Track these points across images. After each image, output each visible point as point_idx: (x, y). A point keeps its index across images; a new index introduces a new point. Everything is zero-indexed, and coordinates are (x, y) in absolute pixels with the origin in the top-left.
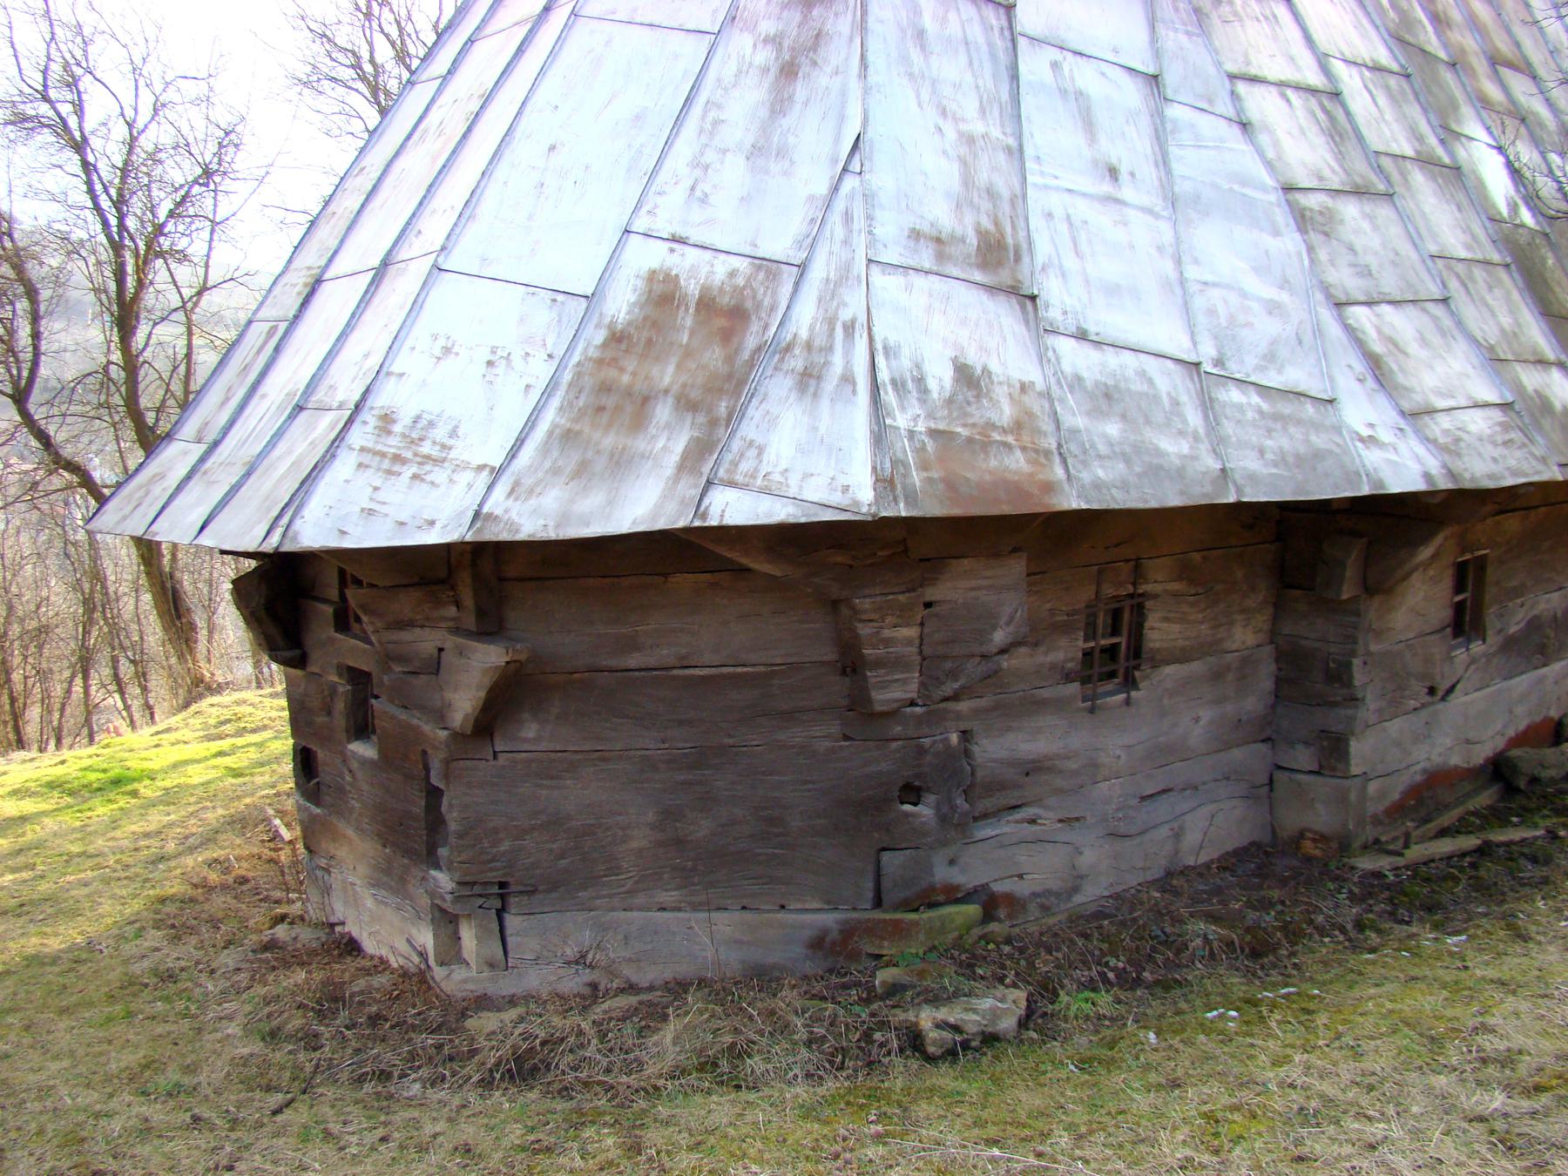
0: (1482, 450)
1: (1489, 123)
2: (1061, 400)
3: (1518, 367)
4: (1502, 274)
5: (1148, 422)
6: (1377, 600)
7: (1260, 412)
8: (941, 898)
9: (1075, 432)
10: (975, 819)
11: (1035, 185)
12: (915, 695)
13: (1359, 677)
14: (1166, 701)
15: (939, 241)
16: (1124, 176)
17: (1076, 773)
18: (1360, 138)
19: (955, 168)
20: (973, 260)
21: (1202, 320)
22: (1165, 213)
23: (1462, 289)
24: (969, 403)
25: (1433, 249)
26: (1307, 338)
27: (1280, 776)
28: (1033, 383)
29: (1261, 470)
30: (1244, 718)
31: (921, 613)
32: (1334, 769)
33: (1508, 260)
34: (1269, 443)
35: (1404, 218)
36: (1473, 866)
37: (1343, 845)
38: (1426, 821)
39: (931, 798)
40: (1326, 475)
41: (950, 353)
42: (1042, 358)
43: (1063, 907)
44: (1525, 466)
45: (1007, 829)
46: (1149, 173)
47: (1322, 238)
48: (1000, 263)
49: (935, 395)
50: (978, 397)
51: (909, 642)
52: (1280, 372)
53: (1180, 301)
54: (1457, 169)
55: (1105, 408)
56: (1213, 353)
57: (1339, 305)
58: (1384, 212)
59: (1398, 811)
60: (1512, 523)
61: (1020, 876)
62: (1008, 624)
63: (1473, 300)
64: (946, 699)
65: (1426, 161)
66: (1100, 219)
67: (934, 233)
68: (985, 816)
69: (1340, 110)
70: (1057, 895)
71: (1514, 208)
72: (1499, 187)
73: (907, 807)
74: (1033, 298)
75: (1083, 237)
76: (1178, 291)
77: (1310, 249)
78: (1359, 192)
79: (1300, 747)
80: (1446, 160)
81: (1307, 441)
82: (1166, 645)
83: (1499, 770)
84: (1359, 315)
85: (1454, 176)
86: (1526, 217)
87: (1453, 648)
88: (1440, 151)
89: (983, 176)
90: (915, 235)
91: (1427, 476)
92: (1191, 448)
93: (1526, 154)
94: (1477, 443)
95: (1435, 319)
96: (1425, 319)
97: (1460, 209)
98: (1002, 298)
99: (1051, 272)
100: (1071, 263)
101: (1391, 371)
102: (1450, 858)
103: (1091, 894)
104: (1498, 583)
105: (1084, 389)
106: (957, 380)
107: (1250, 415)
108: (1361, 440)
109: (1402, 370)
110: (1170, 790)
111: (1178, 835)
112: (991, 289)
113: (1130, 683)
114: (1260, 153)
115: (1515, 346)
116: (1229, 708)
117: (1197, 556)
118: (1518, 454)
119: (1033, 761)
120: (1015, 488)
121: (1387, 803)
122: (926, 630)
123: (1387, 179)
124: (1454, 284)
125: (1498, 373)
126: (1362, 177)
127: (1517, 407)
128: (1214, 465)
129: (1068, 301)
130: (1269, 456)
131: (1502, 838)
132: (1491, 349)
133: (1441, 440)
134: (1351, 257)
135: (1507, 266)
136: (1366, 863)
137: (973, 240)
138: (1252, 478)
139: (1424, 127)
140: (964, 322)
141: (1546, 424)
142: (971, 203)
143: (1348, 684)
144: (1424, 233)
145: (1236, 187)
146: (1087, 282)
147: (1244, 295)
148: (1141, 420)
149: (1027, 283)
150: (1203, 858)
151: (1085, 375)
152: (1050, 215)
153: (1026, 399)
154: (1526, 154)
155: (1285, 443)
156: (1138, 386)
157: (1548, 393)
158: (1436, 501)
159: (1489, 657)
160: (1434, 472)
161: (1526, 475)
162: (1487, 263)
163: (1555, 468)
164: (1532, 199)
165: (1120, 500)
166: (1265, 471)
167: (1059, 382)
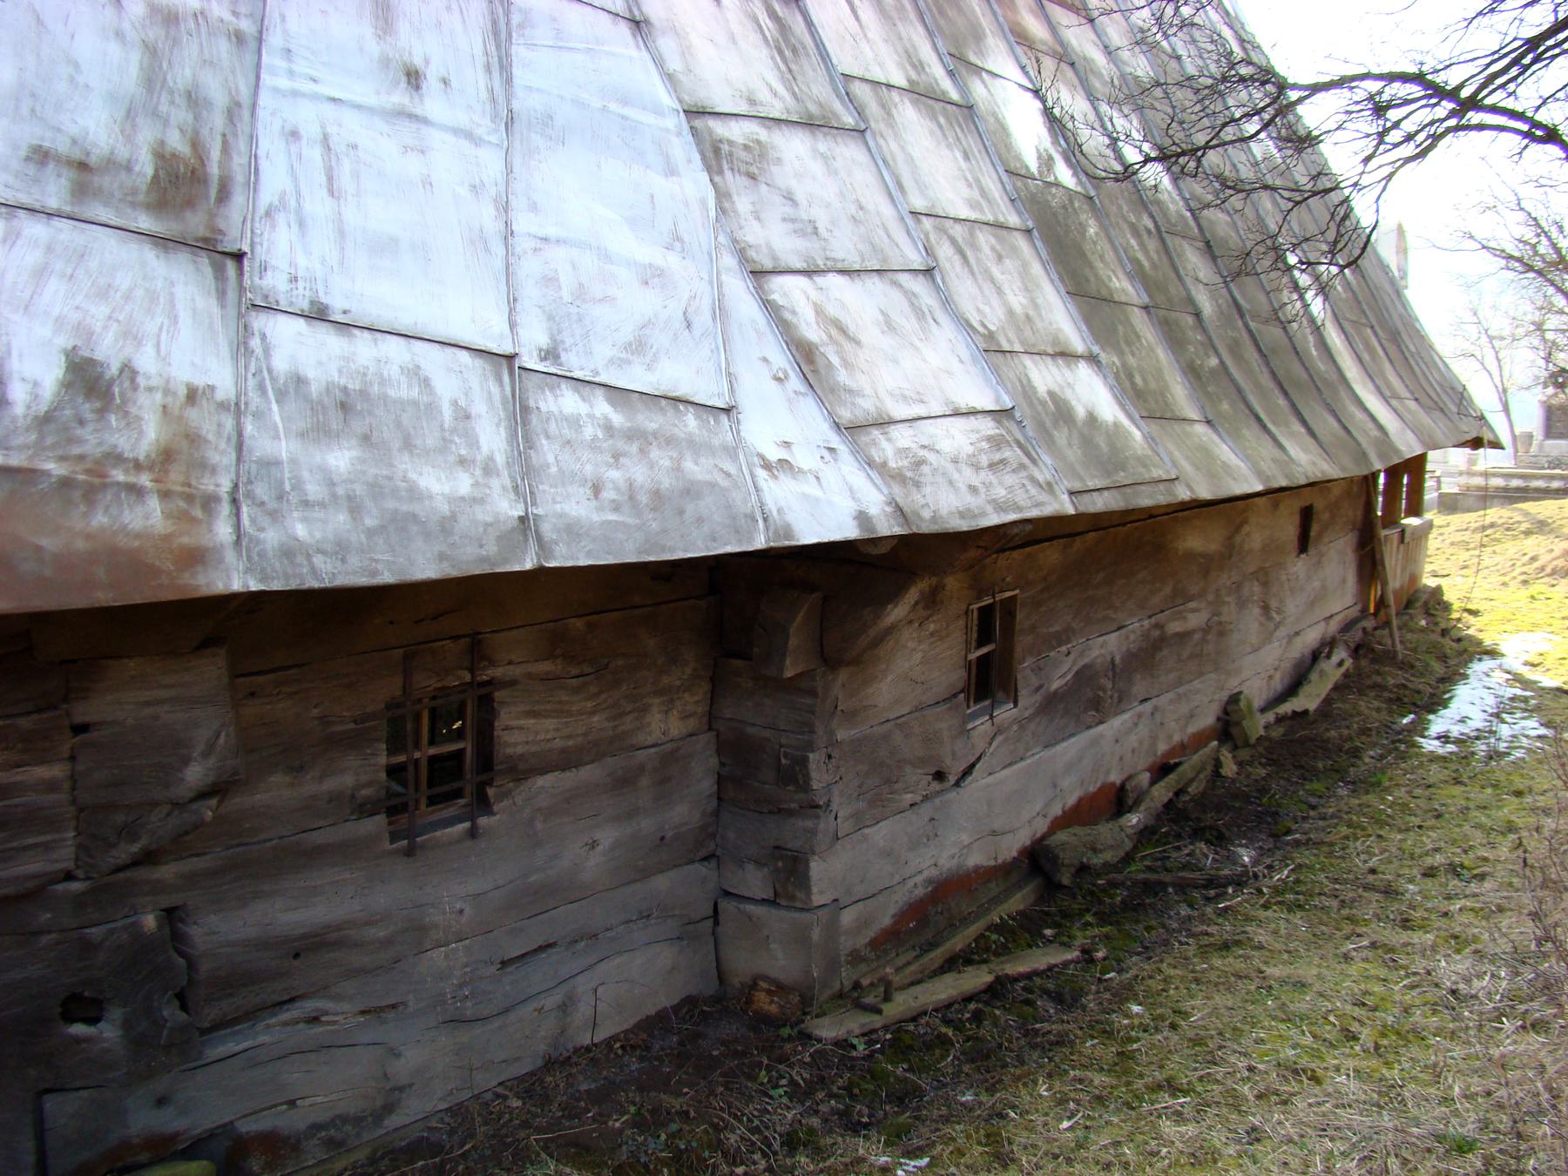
0: (956, 476)
1: (1024, 61)
2: (259, 415)
3: (1027, 361)
4: (1021, 242)
5: (408, 445)
6: (843, 675)
7: (609, 428)
8: (144, 1157)
9: (271, 464)
10: (204, 1032)
11: (276, 90)
12: (71, 865)
13: (819, 776)
14: (539, 826)
15: (83, 166)
16: (431, 83)
17: (388, 942)
18: (824, 56)
19: (136, 57)
20: (141, 198)
21: (530, 294)
22: (493, 139)
23: (957, 258)
24: (82, 422)
25: (919, 204)
26: (703, 319)
27: (727, 906)
28: (212, 388)
29: (590, 512)
30: (669, 835)
31: (67, 744)
32: (792, 898)
33: (1030, 224)
34: (614, 474)
35: (881, 163)
36: (977, 1017)
37: (805, 1001)
38: (932, 945)
39: (116, 1013)
40: (700, 520)
41: (64, 341)
42: (241, 347)
43: (367, 1136)
44: (1020, 497)
45: (262, 1039)
46: (474, 81)
47: (742, 181)
48: (190, 203)
49: (19, 410)
50: (102, 412)
51: (51, 786)
52: (649, 367)
53: (499, 264)
54: (968, 109)
55: (335, 423)
56: (543, 341)
57: (758, 274)
58: (849, 152)
59: (891, 939)
60: (1051, 555)
61: (292, 1103)
62: (206, 755)
63: (972, 273)
64: (136, 863)
65: (922, 94)
66: (382, 145)
67: (77, 155)
68: (216, 1026)
69: (799, 18)
70: (358, 1120)
71: (1047, 163)
72: (1029, 136)
73: (79, 1029)
74: (239, 257)
75: (345, 168)
76: (500, 250)
77: (722, 195)
78: (813, 124)
79: (750, 867)
80: (954, 96)
81: (677, 469)
82: (534, 749)
83: (1036, 861)
84: (791, 291)
85: (965, 117)
86: (1064, 174)
87: (974, 716)
88: (946, 85)
89: (183, 73)
90: (41, 156)
91: (862, 518)
92: (476, 484)
93: (1072, 103)
94: (950, 467)
95: (910, 296)
96: (896, 295)
97: (966, 157)
98: (183, 257)
99: (281, 218)
100: (318, 205)
101: (830, 365)
102: (949, 1006)
103: (412, 1112)
104: (1033, 628)
105: (307, 398)
106: (67, 385)
107: (589, 432)
108: (767, 466)
109: (846, 363)
110: (551, 945)
111: (564, 1008)
112: (163, 242)
113: (483, 804)
114: (659, 62)
115: (1028, 333)
116: (646, 825)
117: (578, 624)
118: (1010, 479)
119: (304, 937)
120: (125, 559)
121: (871, 933)
122: (80, 767)
123: (860, 112)
124: (945, 252)
125: (996, 370)
126: (820, 105)
127: (1017, 415)
128: (510, 509)
129: (302, 262)
130: (608, 494)
131: (1021, 968)
132: (990, 336)
133: (892, 464)
134: (788, 210)
135: (1028, 231)
136: (827, 1029)
137: (146, 167)
138: (572, 530)
139: (926, 52)
140: (103, 293)
141: (1061, 436)
142: (155, 114)
143: (805, 787)
144: (907, 182)
145: (613, 107)
146: (342, 233)
147: (606, 257)
148: (396, 444)
149: (234, 233)
150: (602, 1034)
151: (311, 373)
152: (295, 135)
153: (193, 414)
154: (1072, 103)
155: (640, 474)
156: (404, 391)
157: (1068, 395)
158: (883, 549)
159: (1022, 723)
160: (874, 511)
161: (1020, 509)
162: (998, 226)
163: (1065, 497)
164: (1074, 153)
165: (329, 573)
166: (596, 518)
167: (261, 388)
